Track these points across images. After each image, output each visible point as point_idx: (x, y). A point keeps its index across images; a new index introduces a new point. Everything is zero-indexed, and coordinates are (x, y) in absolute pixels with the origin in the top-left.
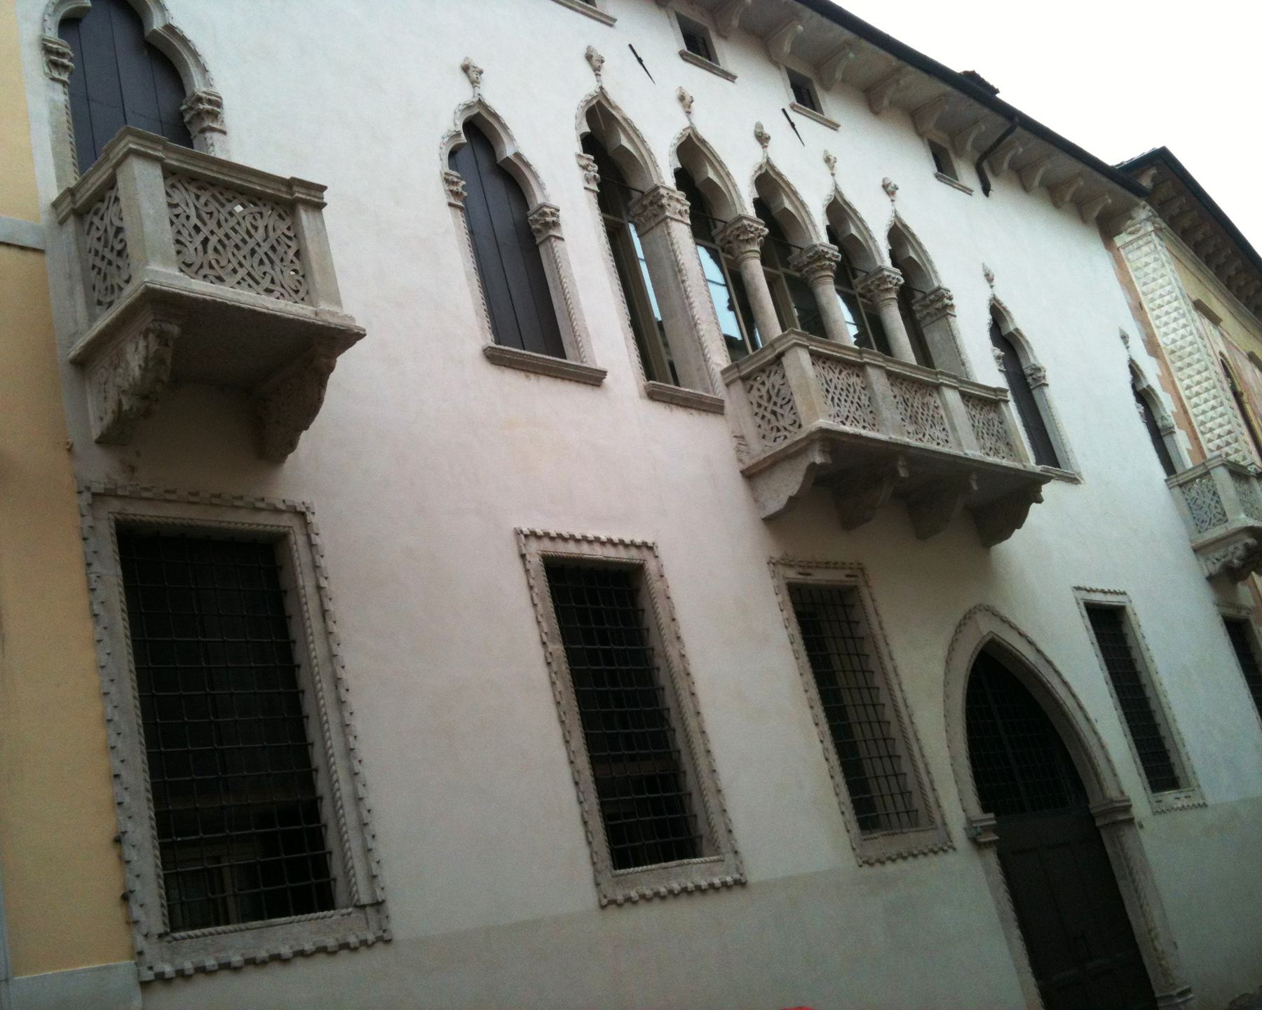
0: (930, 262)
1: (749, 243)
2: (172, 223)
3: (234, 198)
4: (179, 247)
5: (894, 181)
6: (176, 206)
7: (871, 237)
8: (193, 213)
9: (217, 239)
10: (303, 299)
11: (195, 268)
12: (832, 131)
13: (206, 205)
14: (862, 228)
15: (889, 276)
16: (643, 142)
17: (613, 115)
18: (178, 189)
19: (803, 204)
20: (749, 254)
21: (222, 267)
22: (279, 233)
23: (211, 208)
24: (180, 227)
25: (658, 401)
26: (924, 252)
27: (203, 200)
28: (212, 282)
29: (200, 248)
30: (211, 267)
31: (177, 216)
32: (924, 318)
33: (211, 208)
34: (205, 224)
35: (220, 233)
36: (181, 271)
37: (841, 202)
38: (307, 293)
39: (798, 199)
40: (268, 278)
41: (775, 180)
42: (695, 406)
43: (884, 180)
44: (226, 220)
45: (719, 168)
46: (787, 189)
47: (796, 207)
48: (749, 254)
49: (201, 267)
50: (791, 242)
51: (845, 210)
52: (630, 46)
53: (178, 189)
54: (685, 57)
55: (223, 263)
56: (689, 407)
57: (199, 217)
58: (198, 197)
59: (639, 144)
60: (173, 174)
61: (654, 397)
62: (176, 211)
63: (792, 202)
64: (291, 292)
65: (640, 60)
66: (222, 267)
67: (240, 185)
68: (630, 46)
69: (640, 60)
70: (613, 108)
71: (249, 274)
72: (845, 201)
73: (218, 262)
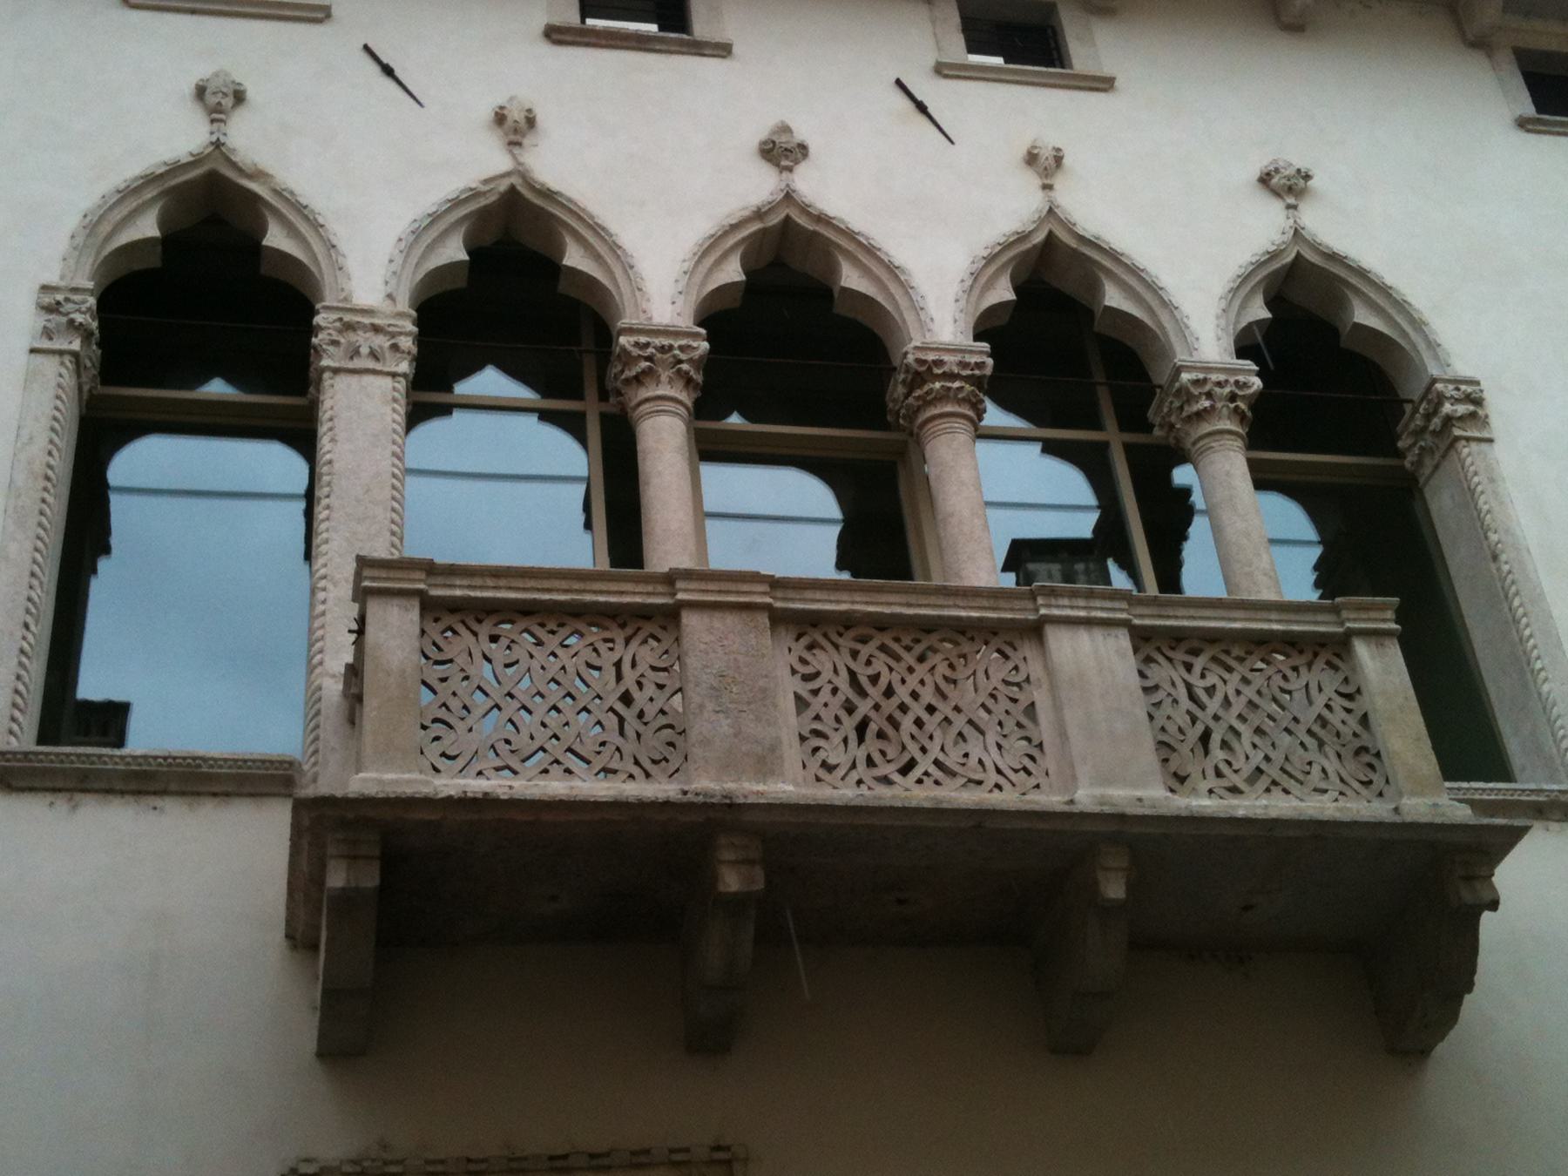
0: (1418, 324)
1: (1204, 420)
2: (1151, 717)
3: (1249, 653)
4: (1165, 753)
5: (1295, 157)
6: (1156, 687)
7: (1166, 304)
8: (1182, 693)
9: (1225, 726)
10: (1381, 794)
11: (841, 772)
12: (1102, 95)
13: (869, 663)
14: (1140, 288)
15: (1196, 382)
16: (317, 226)
17: (249, 191)
18: (1157, 662)
19: (892, 269)
20: (646, 407)
21: (1236, 771)
22: (995, 681)
23: (1212, 679)
24: (1003, 717)
25: (31, 789)
26: (1402, 306)
27: (1197, 669)
28: (1221, 798)
29: (853, 737)
30: (1219, 774)
31: (1158, 705)
32: (1419, 463)
33: (1212, 679)
34: (1202, 707)
35: (890, 706)
36: (1172, 791)
37: (1073, 243)
38: (1387, 781)
39: (880, 261)
40: (1316, 770)
41: (815, 233)
42: (173, 787)
43: (1035, 140)
44: (903, 681)
45: (592, 239)
46: (851, 247)
47: (598, 258)
48: (641, 408)
49: (854, 766)
50: (1403, 396)
51: (1089, 259)
52: (366, 48)
53: (1157, 662)
54: (555, 36)
55: (891, 754)
56: (147, 793)
57: (1192, 697)
58: (1189, 667)
59: (1148, 296)
60: (1147, 639)
61: (14, 783)
62: (1156, 698)
63: (866, 272)
64: (1356, 785)
65: (388, 71)
66: (1236, 771)
67: (1011, 619)
68: (366, 48)
69: (388, 71)
70: (250, 177)
71: (937, 763)
72: (1082, 239)
73: (883, 753)
